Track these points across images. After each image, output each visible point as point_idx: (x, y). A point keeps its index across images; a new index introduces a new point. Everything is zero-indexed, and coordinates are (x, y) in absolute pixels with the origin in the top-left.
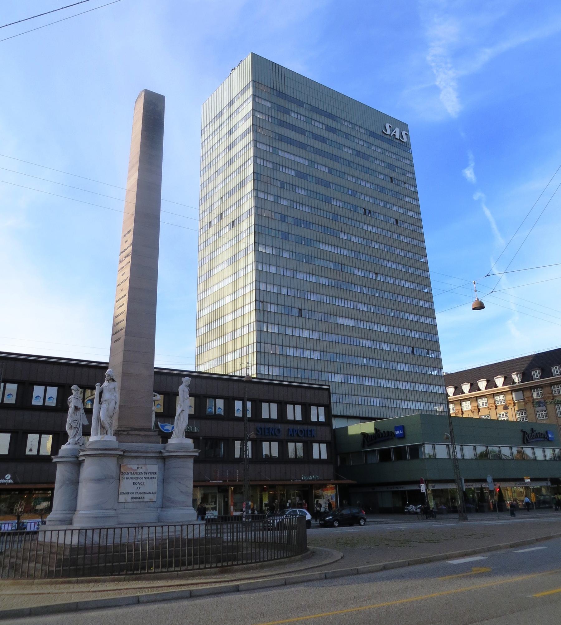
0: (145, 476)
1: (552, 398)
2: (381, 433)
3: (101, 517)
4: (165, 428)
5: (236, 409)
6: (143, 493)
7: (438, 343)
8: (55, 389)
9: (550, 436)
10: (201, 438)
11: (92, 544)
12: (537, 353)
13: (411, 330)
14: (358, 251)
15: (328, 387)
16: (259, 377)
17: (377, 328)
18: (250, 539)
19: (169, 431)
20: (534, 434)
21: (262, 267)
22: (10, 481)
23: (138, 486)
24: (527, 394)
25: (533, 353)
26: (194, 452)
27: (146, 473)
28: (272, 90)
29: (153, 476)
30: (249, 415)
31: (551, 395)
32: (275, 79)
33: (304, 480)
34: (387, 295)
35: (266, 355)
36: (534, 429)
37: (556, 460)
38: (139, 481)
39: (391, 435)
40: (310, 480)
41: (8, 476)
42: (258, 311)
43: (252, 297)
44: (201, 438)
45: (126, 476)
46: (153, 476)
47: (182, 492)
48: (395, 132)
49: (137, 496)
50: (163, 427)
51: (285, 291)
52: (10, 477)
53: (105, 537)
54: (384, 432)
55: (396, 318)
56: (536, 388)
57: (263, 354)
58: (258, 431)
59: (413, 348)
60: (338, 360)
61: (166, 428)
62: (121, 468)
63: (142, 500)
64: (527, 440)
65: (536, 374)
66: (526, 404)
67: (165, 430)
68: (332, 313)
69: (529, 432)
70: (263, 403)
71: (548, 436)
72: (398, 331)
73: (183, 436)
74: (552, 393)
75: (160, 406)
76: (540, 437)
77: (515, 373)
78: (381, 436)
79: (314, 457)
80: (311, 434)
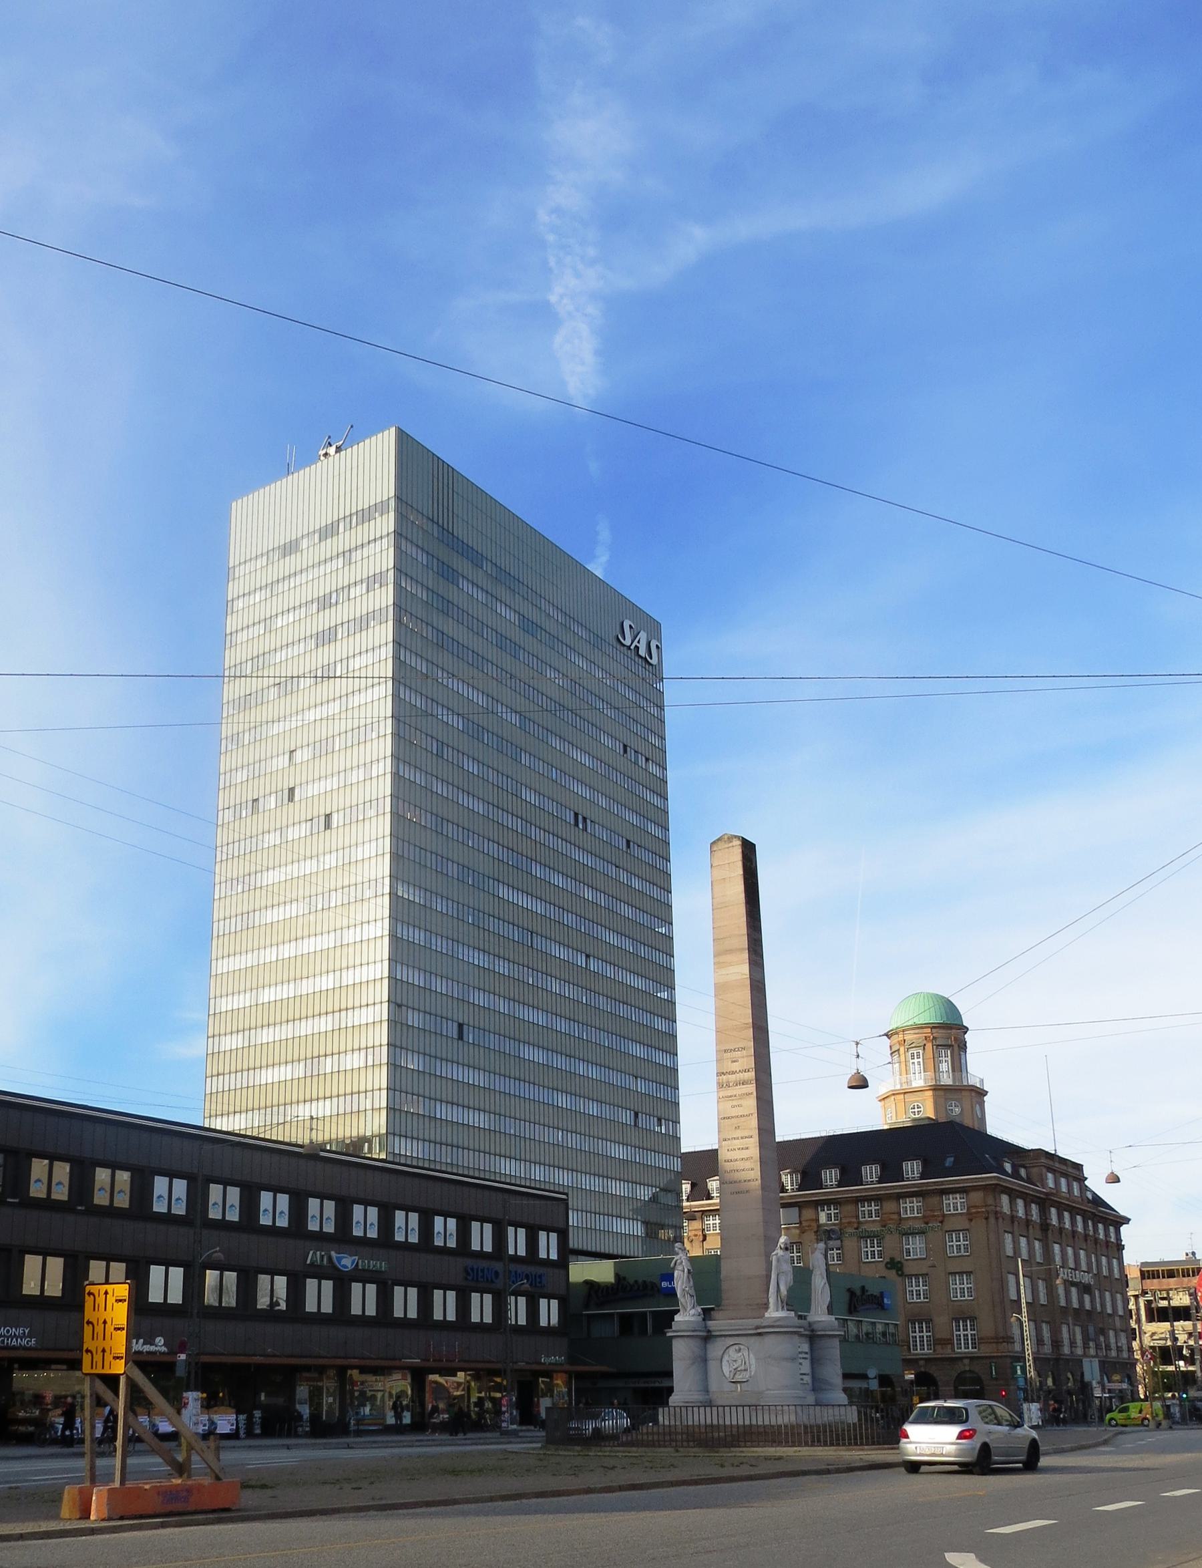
1: (855, 1225)
4: (342, 1263)
5: (436, 1232)
7: (676, 1104)
8: (67, 1167)
9: (886, 1301)
12: (832, 1134)
13: (636, 1078)
15: (564, 1197)
16: (390, 1159)
17: (582, 1069)
19: (347, 1267)
20: (864, 1297)
21: (400, 931)
22: (164, 1349)
24: (808, 1213)
25: (824, 1134)
28: (430, 523)
31: (854, 1220)
32: (436, 498)
33: (544, 1364)
34: (602, 1003)
35: (403, 1115)
36: (866, 1288)
37: (889, 1344)
40: (553, 1364)
41: (160, 1341)
42: (393, 1024)
43: (382, 992)
48: (639, 642)
50: (339, 1260)
51: (440, 986)
54: (636, 1282)
56: (820, 1205)
57: (397, 1113)
58: (468, 1274)
59: (636, 1115)
60: (512, 1132)
61: (344, 1262)
64: (855, 1307)
65: (830, 1176)
66: (803, 1232)
68: (512, 1036)
69: (858, 1293)
70: (156, 1177)
72: (616, 1079)
74: (857, 1217)
75: (61, 1186)
77: (788, 1171)
79: (396, 1315)
80: (540, 1282)
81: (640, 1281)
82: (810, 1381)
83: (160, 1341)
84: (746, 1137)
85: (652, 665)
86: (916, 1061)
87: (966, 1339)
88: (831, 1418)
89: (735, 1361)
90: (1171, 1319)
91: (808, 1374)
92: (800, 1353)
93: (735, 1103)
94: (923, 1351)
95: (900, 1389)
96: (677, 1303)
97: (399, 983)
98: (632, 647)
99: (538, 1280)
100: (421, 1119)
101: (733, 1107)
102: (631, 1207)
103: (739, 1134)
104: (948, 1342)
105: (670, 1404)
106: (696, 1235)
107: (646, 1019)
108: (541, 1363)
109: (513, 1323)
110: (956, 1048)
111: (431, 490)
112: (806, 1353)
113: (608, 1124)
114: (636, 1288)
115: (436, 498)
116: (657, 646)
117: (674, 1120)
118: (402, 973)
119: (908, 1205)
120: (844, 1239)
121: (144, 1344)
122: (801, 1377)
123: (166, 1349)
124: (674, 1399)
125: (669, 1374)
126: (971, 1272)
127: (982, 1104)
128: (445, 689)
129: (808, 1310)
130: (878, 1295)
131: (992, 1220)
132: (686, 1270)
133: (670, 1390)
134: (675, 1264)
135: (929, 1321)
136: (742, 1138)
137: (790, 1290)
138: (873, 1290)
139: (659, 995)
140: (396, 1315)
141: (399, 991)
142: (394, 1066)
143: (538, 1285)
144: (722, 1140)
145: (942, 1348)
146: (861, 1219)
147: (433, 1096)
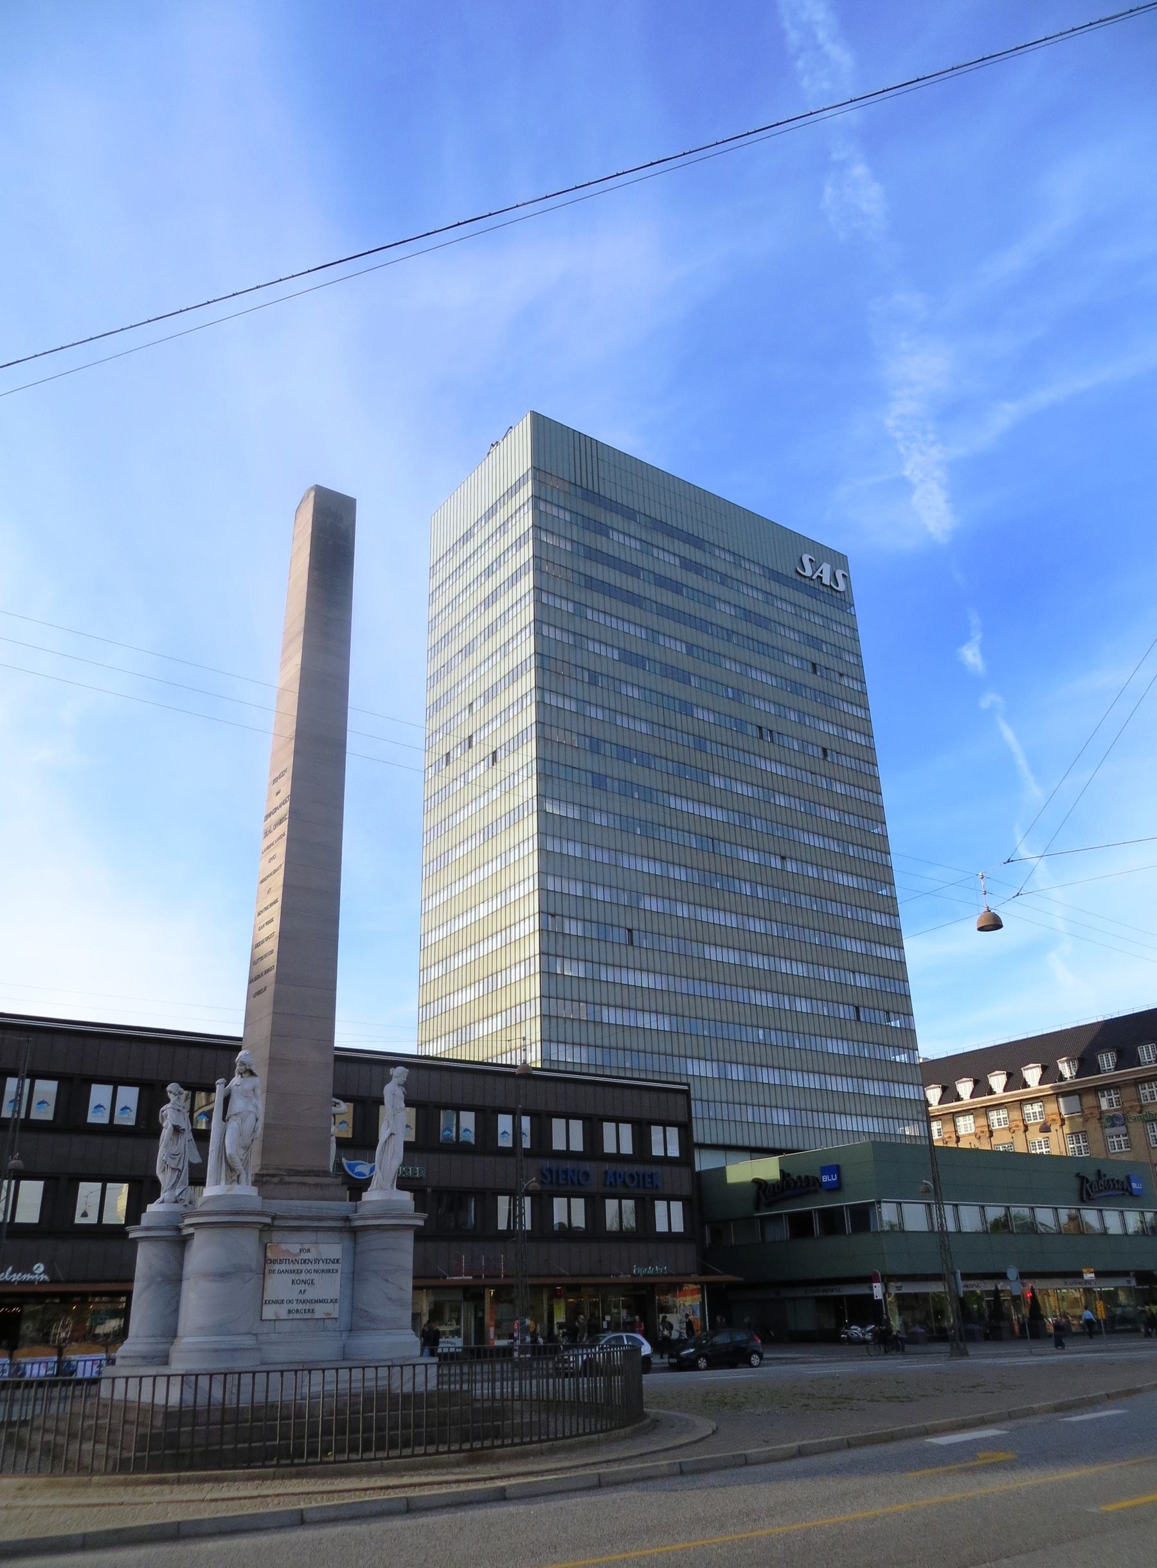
0: (316, 1267)
1: (1138, 1109)
3: (227, 1350)
5: (500, 1131)
6: (311, 1302)
7: (908, 997)
9: (1134, 1185)
10: (429, 1190)
15: (686, 1088)
16: (547, 1066)
18: (528, 1393)
20: (1101, 1182)
22: (44, 1277)
23: (302, 1287)
24: (1089, 1100)
25: (1100, 1019)
27: (317, 1261)
28: (572, 487)
29: (331, 1266)
30: (526, 1143)
33: (637, 1275)
34: (804, 901)
36: (1103, 1172)
38: (303, 1277)
41: (39, 1268)
44: (429, 1190)
45: (277, 1267)
46: (331, 1266)
47: (390, 1299)
48: (821, 572)
49: (300, 1307)
50: (352, 1167)
51: (599, 894)
52: (42, 1268)
53: (235, 1390)
54: (799, 1177)
55: (824, 948)
57: (554, 1021)
59: (857, 1008)
60: (706, 1033)
61: (358, 1169)
62: (268, 1251)
63: (309, 1316)
64: (1088, 1194)
65: (1107, 1060)
66: (1086, 1121)
67: (356, 1174)
69: (1092, 1177)
71: (1130, 1186)
73: (392, 1185)
74: (1139, 1100)
77: (1065, 1059)
79: (500, 1228)
80: (652, 1182)
83: (39, 1268)
85: (840, 592)
88: (370, 1384)
90: (12, 1121)
97: (551, 894)
98: (814, 577)
100: (584, 1026)
106: (983, 1132)
107: (862, 915)
111: (572, 457)
113: (843, 1025)
115: (578, 465)
116: (844, 575)
117: (906, 1012)
118: (891, 954)
120: (1129, 1125)
121: (11, 1273)
123: (46, 1278)
128: (596, 625)
140: (500, 1228)
142: (547, 974)
147: (597, 1000)
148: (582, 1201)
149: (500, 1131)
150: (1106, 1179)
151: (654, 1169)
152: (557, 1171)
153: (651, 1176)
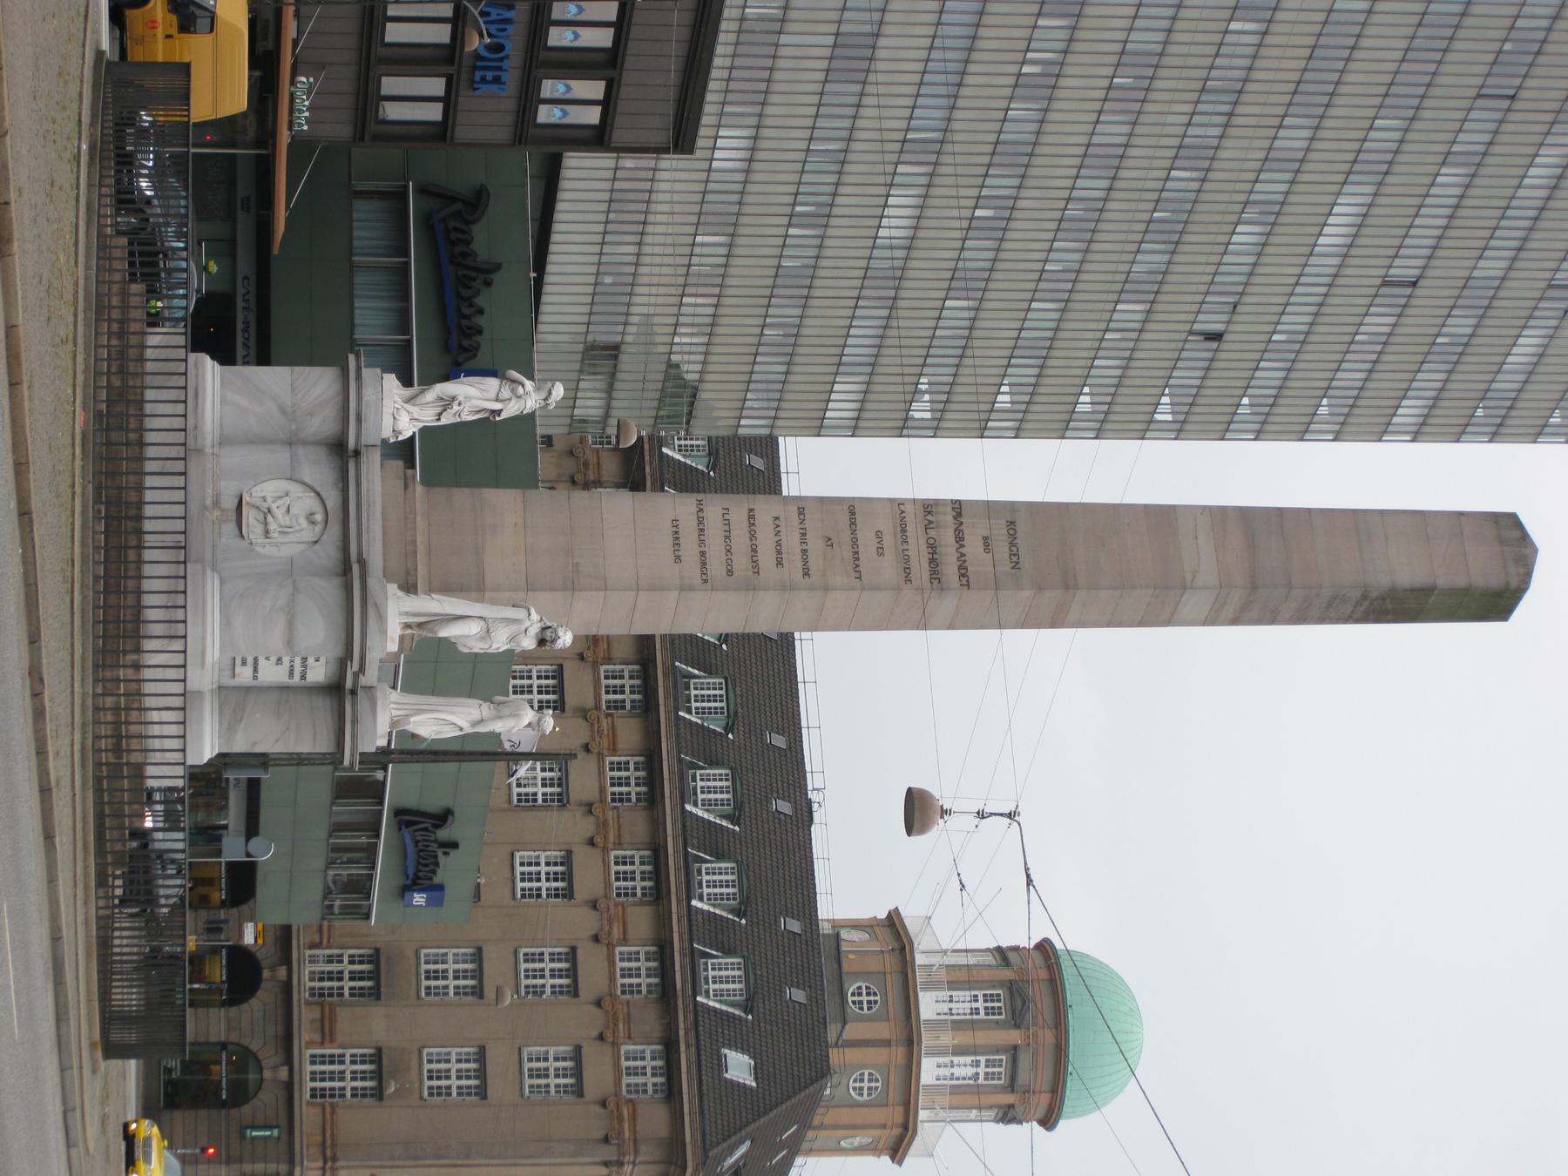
2: (478, 293)
11: (143, 680)
14: (1396, 168)
26: (352, 755)
33: (293, 83)
36: (453, 853)
39: (466, 350)
54: (480, 332)
55: (1022, 315)
64: (409, 824)
69: (443, 834)
71: (420, 891)
73: (407, 614)
76: (419, 863)
78: (465, 293)
80: (483, 80)
81: (481, 321)
82: (238, 681)
84: (805, 562)
86: (980, 1004)
87: (330, 976)
89: (288, 510)
91: (255, 678)
92: (305, 659)
93: (888, 540)
94: (308, 969)
95: (222, 917)
96: (429, 381)
99: (490, 75)
101: (879, 534)
102: (657, 320)
103: (815, 543)
104: (326, 1031)
105: (192, 357)
108: (294, 74)
109: (390, 13)
110: (1009, 1099)
112: (303, 677)
114: (466, 311)
119: (627, 682)
122: (250, 660)
124: (208, 369)
125: (264, 359)
126: (484, 1097)
127: (872, 1149)
129: (409, 688)
130: (437, 880)
131: (609, 1153)
132: (497, 406)
133: (225, 357)
134: (514, 381)
135: (375, 994)
136: (804, 551)
137: (448, 644)
138: (450, 869)
139: (1165, 400)
141: (1206, 13)
143: (478, 75)
144: (802, 506)
145: (313, 1021)
146: (603, 668)
148: (446, 39)
149: (572, 83)
150: (440, 853)
151: (512, 77)
152: (500, 69)
153: (497, 80)
